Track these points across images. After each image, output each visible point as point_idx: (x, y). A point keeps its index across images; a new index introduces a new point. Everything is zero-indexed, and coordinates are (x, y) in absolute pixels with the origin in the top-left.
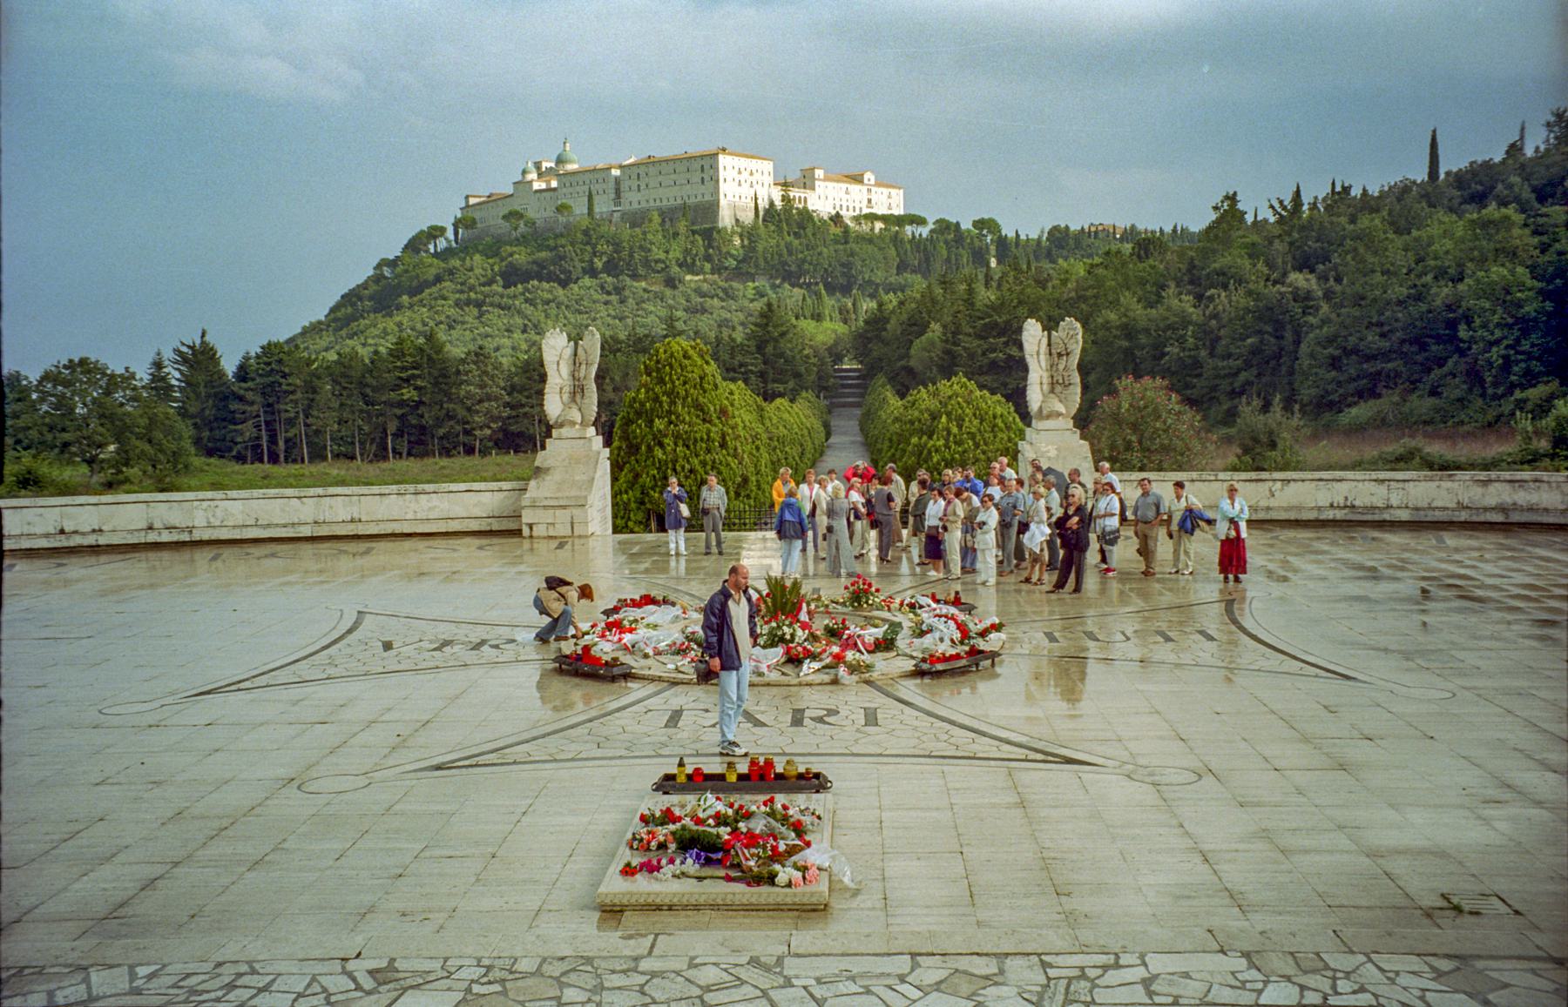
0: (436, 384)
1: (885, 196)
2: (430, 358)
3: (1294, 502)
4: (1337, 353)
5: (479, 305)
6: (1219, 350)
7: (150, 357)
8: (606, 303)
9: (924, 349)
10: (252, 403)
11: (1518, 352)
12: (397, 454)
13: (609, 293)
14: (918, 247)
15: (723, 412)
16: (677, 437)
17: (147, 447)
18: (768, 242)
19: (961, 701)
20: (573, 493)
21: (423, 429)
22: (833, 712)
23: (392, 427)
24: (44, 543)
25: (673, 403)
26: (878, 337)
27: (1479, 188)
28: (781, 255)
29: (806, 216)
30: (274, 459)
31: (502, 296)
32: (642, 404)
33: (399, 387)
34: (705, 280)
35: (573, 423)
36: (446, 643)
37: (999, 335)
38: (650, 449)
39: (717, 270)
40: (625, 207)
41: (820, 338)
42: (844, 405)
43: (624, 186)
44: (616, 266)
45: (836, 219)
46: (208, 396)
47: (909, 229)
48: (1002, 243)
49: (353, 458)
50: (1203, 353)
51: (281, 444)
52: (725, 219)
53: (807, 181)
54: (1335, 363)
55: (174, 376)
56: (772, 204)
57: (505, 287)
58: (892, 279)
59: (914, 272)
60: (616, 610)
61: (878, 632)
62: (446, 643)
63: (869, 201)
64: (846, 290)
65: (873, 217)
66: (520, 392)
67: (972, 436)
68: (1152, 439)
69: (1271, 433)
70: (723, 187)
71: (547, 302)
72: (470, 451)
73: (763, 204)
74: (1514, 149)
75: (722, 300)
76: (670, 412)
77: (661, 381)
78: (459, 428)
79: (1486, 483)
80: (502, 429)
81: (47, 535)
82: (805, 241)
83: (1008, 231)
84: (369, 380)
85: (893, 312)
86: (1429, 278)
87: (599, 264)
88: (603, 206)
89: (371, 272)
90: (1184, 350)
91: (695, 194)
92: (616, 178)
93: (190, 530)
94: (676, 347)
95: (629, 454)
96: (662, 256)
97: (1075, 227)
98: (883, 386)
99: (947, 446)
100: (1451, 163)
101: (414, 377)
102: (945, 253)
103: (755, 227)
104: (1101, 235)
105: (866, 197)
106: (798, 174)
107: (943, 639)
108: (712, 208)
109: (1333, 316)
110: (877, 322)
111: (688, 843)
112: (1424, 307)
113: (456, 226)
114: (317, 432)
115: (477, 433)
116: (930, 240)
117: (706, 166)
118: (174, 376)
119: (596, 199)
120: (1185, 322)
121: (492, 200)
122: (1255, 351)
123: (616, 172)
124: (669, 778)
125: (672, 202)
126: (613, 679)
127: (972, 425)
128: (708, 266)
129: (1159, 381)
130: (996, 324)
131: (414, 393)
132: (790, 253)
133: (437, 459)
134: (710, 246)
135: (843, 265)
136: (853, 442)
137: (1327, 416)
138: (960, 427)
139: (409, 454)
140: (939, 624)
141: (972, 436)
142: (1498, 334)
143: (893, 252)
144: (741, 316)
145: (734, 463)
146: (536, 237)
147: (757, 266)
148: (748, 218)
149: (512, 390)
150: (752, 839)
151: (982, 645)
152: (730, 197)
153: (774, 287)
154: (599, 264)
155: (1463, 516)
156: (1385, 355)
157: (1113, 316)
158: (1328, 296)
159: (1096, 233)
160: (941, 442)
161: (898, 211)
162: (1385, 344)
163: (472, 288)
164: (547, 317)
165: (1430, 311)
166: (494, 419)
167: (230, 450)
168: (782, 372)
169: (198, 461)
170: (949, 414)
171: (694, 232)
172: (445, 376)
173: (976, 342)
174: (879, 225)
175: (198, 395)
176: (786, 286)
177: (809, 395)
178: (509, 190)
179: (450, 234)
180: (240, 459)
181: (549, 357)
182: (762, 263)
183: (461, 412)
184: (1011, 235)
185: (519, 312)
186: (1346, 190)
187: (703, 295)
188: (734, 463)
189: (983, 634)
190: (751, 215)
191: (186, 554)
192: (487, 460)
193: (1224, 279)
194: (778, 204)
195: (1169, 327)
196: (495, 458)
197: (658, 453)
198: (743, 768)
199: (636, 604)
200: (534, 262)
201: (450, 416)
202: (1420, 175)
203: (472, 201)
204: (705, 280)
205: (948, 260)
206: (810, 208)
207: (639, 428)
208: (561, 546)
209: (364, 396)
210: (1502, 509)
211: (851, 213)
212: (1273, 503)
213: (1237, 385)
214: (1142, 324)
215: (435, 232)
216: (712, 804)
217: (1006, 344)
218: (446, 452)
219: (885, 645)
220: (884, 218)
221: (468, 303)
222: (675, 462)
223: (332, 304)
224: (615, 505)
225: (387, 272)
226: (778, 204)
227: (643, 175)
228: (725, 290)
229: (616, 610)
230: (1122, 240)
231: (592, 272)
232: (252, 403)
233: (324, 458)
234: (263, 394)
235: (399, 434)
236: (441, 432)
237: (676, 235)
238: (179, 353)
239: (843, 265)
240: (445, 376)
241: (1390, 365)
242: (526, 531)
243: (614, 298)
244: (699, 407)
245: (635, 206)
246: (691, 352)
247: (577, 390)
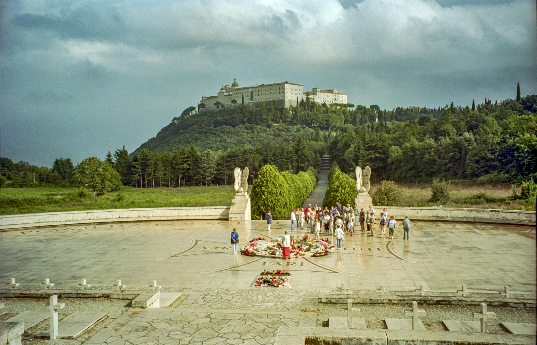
0: (194, 163)
2: (192, 155)
3: (423, 215)
4: (478, 159)
5: (206, 133)
6: (442, 156)
7: (107, 153)
8: (247, 133)
9: (349, 154)
10: (138, 168)
11: (533, 161)
12: (182, 185)
13: (248, 130)
14: (351, 114)
15: (281, 185)
16: (268, 192)
17: (110, 184)
18: (301, 113)
19: (320, 261)
20: (242, 210)
21: (190, 177)
22: (295, 263)
23: (180, 176)
24: (116, 220)
25: (267, 183)
26: (335, 148)
27: (530, 104)
28: (305, 117)
29: (314, 104)
30: (144, 186)
31: (213, 130)
32: (259, 183)
33: (183, 164)
34: (280, 125)
35: (241, 192)
36: (217, 248)
37: (373, 150)
38: (261, 195)
39: (284, 122)
41: (317, 147)
42: (324, 169)
44: (251, 120)
45: (324, 105)
46: (125, 166)
47: (348, 108)
48: (380, 113)
49: (168, 186)
50: (436, 157)
51: (146, 181)
52: (287, 105)
53: (314, 92)
54: (477, 162)
55: (114, 160)
56: (303, 100)
57: (215, 127)
58: (343, 126)
59: (350, 123)
60: (252, 241)
61: (307, 247)
62: (217, 248)
63: (335, 99)
64: (327, 129)
65: (336, 105)
66: (220, 166)
67: (348, 193)
68: (390, 197)
69: (441, 189)
70: (286, 95)
71: (228, 133)
72: (204, 184)
73: (300, 100)
75: (286, 132)
76: (266, 185)
77: (264, 177)
78: (201, 177)
79: (471, 211)
80: (214, 177)
81: (117, 218)
82: (313, 113)
83: (382, 109)
84: (174, 162)
85: (340, 140)
86: (508, 136)
87: (245, 120)
88: (247, 101)
89: (171, 122)
90: (430, 156)
91: (277, 97)
93: (149, 217)
94: (268, 168)
95: (255, 196)
96: (266, 117)
97: (405, 108)
98: (335, 165)
99: (341, 195)
100: (523, 95)
101: (188, 161)
102: (360, 116)
103: (297, 108)
104: (414, 110)
105: (334, 97)
106: (311, 90)
107: (321, 249)
108: (283, 102)
109: (477, 147)
110: (335, 143)
111: (265, 282)
112: (506, 145)
113: (199, 107)
114: (157, 178)
115: (207, 178)
116: (356, 112)
117: (280, 87)
118: (114, 160)
119: (245, 98)
120: (431, 147)
122: (453, 157)
124: (263, 273)
125: (270, 99)
126: (252, 256)
127: (348, 189)
128: (281, 121)
129: (392, 182)
130: (372, 146)
131: (188, 166)
132: (308, 116)
133: (194, 187)
134: (282, 114)
135: (326, 121)
136: (326, 183)
137: (474, 179)
138: (344, 190)
139: (185, 185)
140: (320, 246)
141: (348, 193)
142: (527, 155)
143: (343, 116)
144: (292, 138)
145: (283, 199)
146: (226, 111)
147: (297, 121)
149: (218, 165)
150: (275, 281)
151: (329, 250)
152: (289, 98)
153: (303, 128)
154: (245, 120)
155: (465, 220)
156: (493, 160)
157: (408, 145)
158: (476, 140)
159: (412, 110)
160: (339, 194)
161: (345, 102)
162: (493, 157)
163: (204, 127)
164: (228, 137)
165: (508, 146)
166: (212, 174)
167: (131, 183)
168: (303, 160)
169: (122, 187)
170: (342, 186)
171: (277, 110)
172: (197, 161)
173: (365, 152)
174: (338, 107)
175: (122, 166)
176: (307, 127)
177: (311, 168)
178: (217, 95)
179: (197, 109)
180: (134, 186)
181: (236, 175)
182: (299, 120)
183: (202, 172)
184: (383, 110)
185: (219, 136)
186: (489, 102)
187: (279, 130)
188: (283, 199)
189: (330, 248)
190: (296, 104)
191: (148, 223)
192: (210, 187)
193: (445, 133)
194: (305, 100)
195: (426, 149)
196: (212, 187)
197: (263, 196)
198: (276, 272)
199: (257, 240)
200: (224, 119)
201: (199, 173)
202: (514, 98)
203: (204, 99)
204: (280, 125)
205: (361, 119)
206: (315, 101)
207: (258, 190)
208: (239, 223)
209: (172, 166)
210: (474, 218)
211: (329, 103)
212: (418, 215)
213: (447, 168)
214: (418, 147)
215: (193, 109)
216: (269, 276)
217: (375, 152)
218: (197, 184)
219: (308, 250)
220: (340, 105)
221: (202, 132)
222: (267, 198)
223: (158, 132)
224: (251, 210)
225: (176, 122)
226: (305, 100)
228: (286, 129)
229: (252, 241)
230: (421, 112)
231: (243, 123)
232: (138, 168)
233: (159, 186)
234: (142, 166)
235: (182, 179)
236: (196, 178)
237: (271, 110)
238: (116, 152)
239: (326, 121)
240: (197, 161)
241: (494, 163)
242: (230, 219)
243: (250, 131)
244: (274, 184)
245: (257, 101)
246: (272, 169)
247: (242, 184)
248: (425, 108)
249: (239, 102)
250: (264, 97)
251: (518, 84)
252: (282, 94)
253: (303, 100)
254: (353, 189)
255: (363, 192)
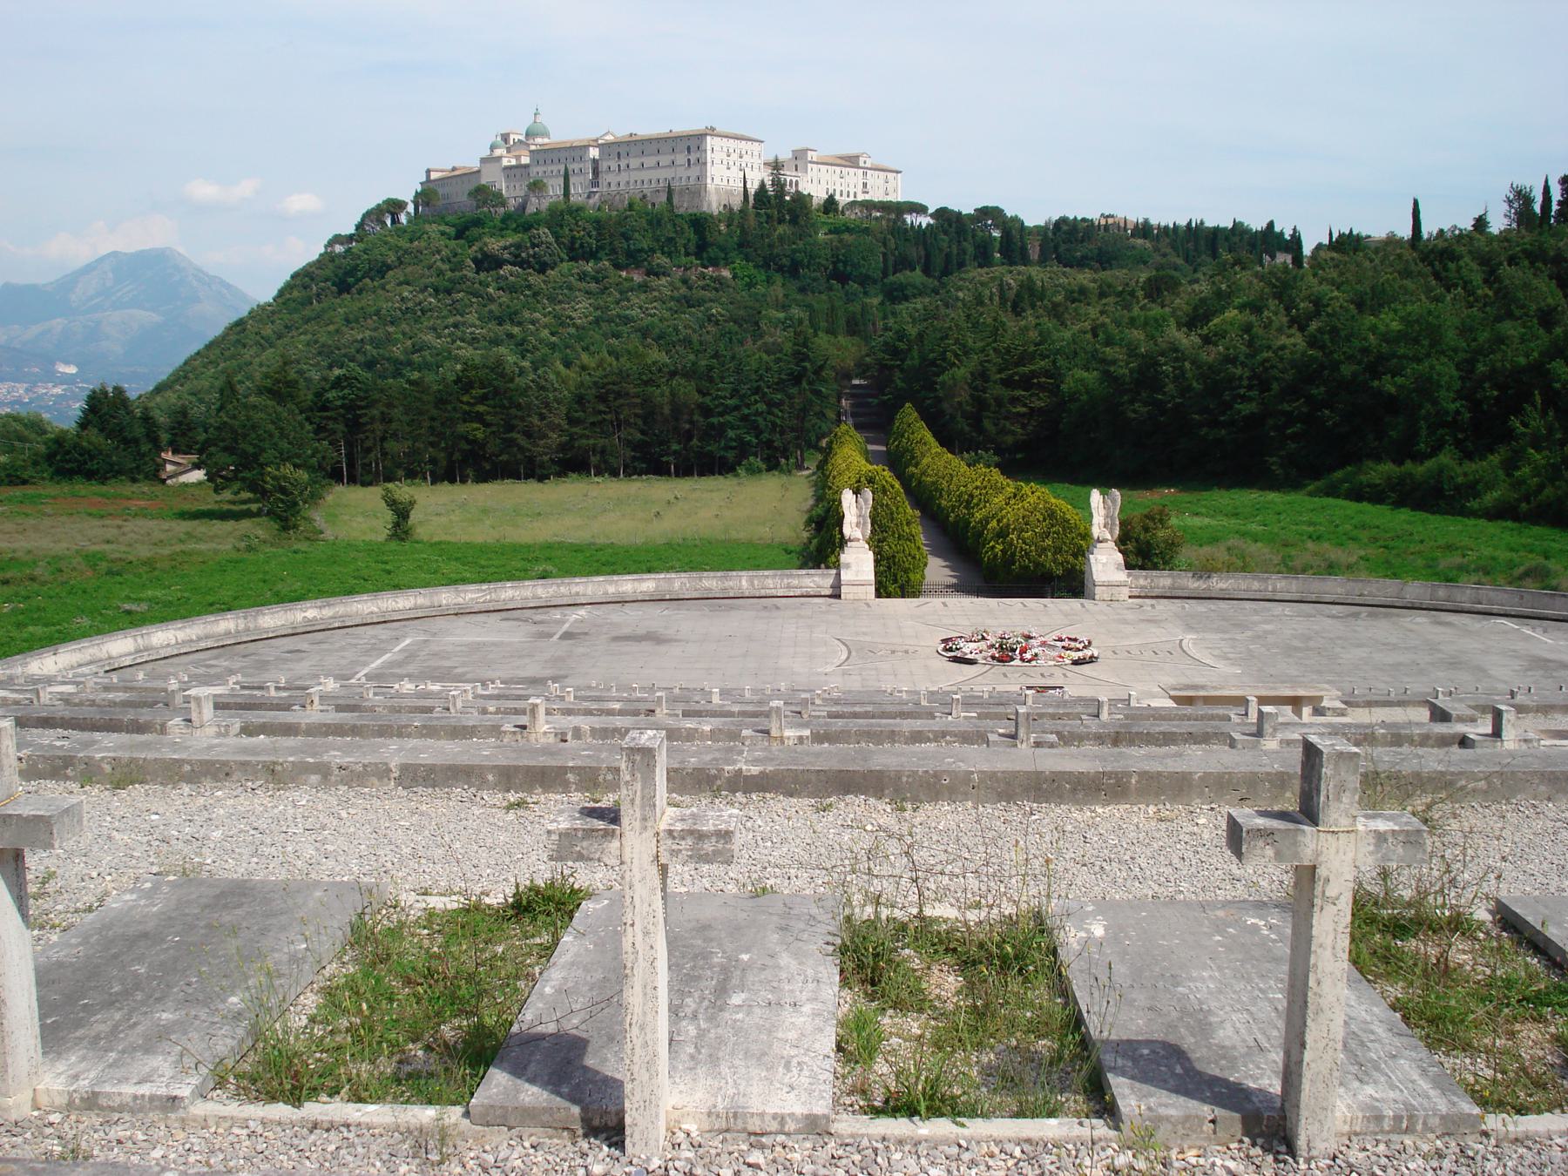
1: (881, 181)
29: (801, 200)
40: (603, 188)
43: (603, 166)
45: (830, 204)
47: (908, 218)
63: (865, 185)
70: (711, 170)
73: (753, 187)
74: (1481, 223)
88: (578, 193)
91: (682, 176)
92: (594, 161)
100: (1429, 228)
108: (698, 190)
119: (572, 180)
121: (457, 178)
123: (594, 153)
148: (737, 203)
179: (411, 208)
194: (768, 183)
202: (1405, 232)
203: (434, 176)
215: (394, 207)
226: (768, 183)
227: (623, 154)
248: (1146, 221)
249: (554, 189)
250: (635, 176)
251: (1416, 203)
252: (694, 172)
253: (763, 185)
254: (1086, 535)
255: (1105, 541)
